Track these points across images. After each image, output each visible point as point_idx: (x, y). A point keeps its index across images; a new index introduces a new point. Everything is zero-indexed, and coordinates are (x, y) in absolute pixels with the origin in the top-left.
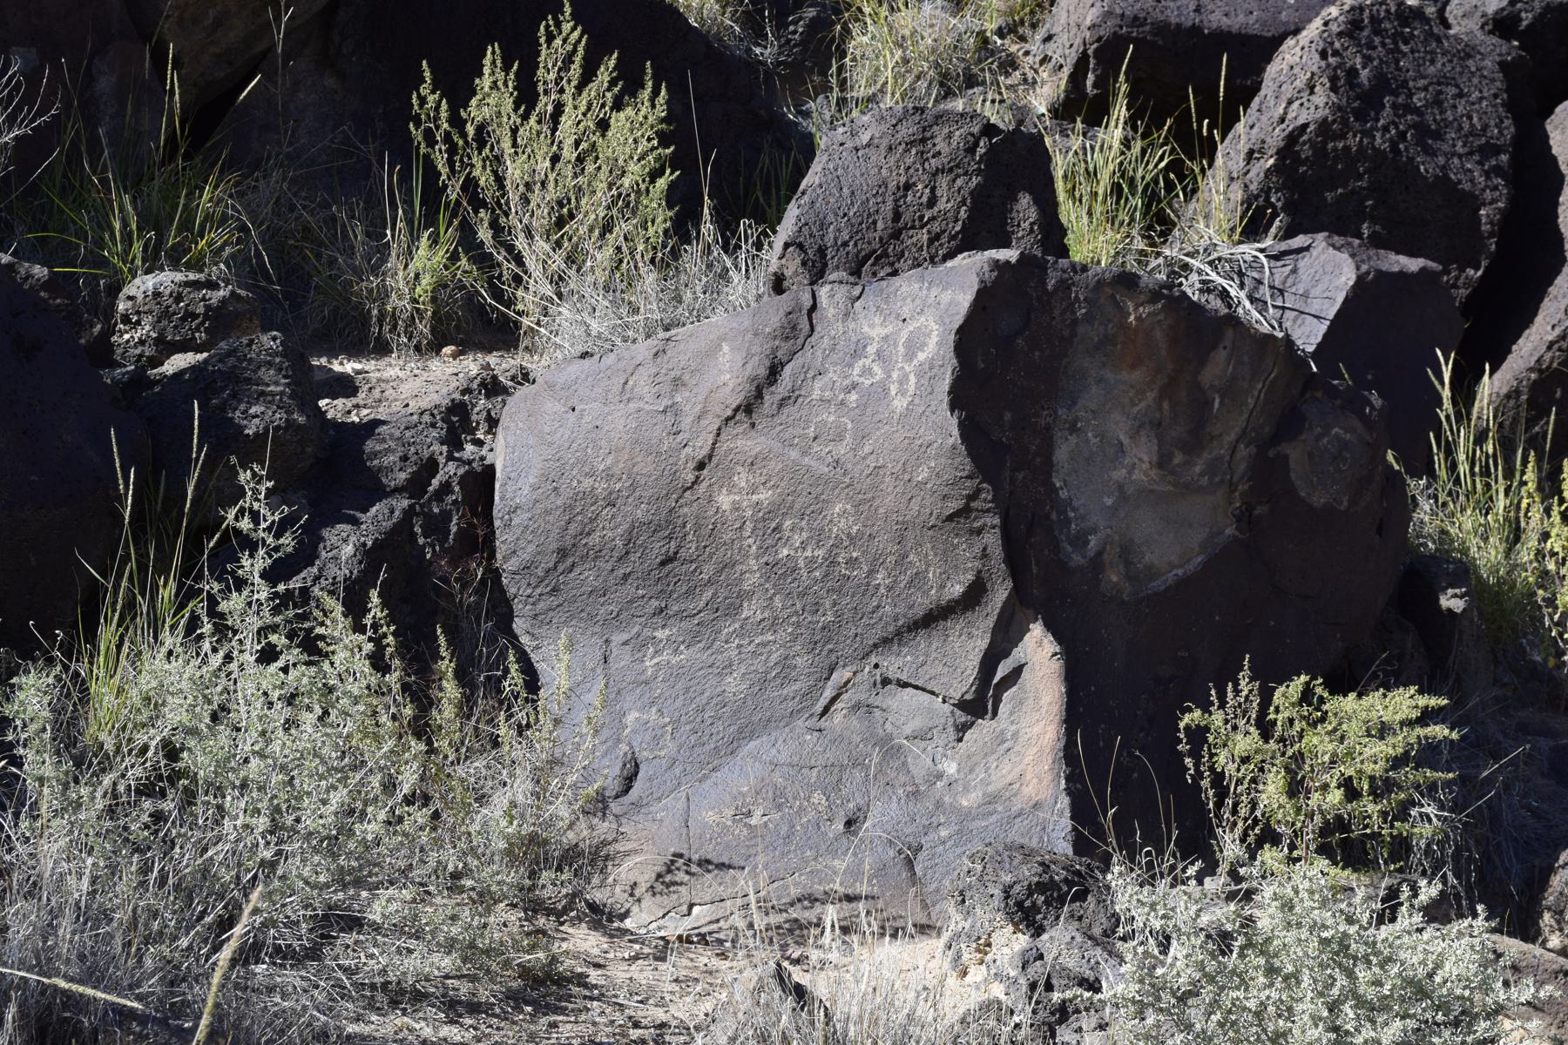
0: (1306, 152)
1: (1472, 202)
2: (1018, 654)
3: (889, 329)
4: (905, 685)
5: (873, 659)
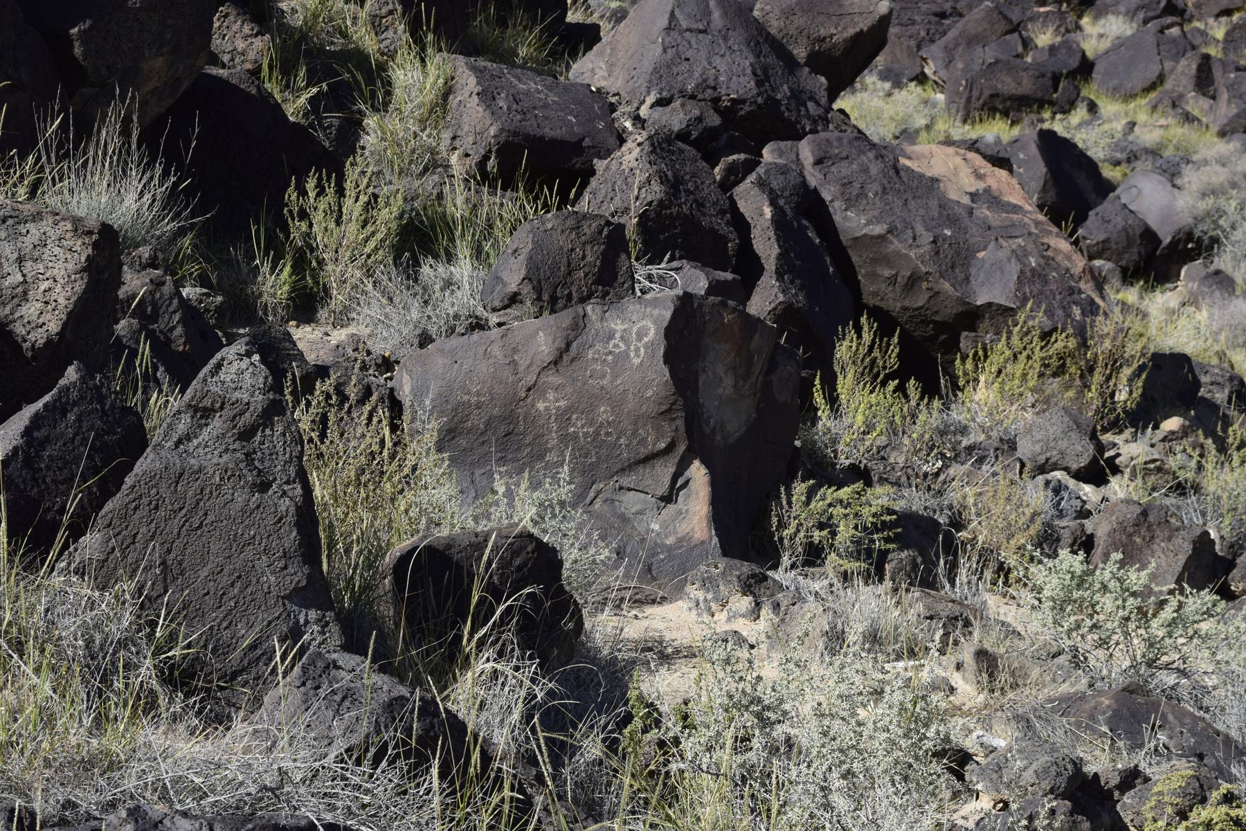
0: (652, 215)
1: (725, 240)
2: (687, 473)
3: (625, 326)
4: (630, 489)
5: (615, 478)
